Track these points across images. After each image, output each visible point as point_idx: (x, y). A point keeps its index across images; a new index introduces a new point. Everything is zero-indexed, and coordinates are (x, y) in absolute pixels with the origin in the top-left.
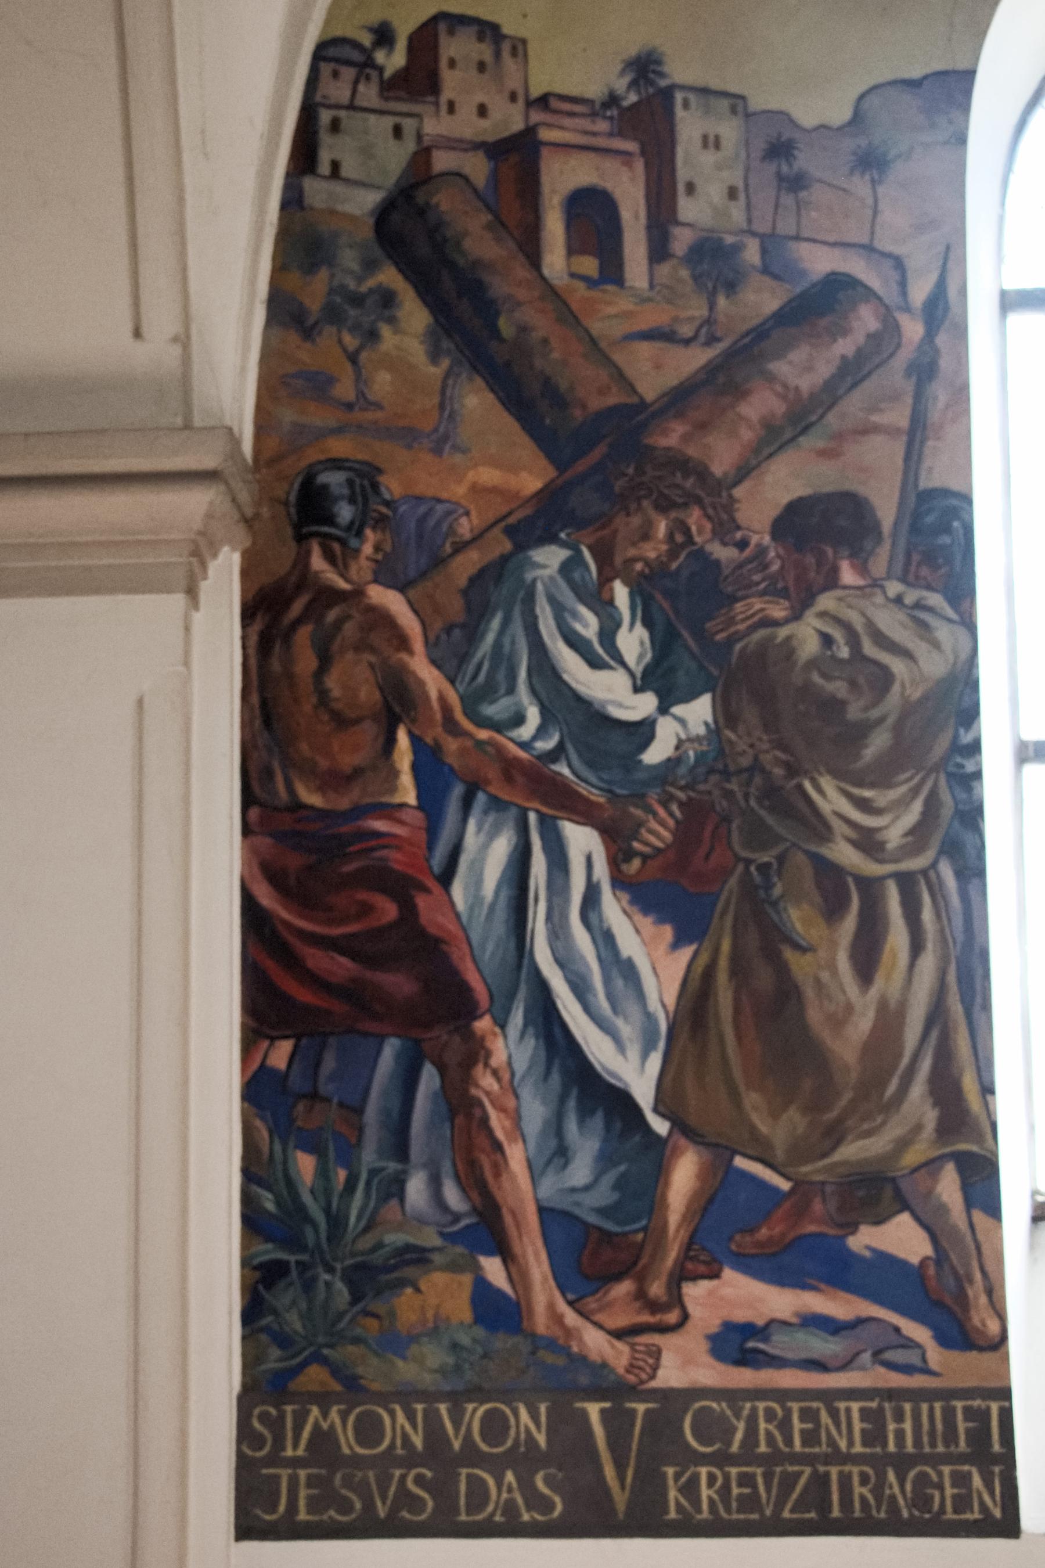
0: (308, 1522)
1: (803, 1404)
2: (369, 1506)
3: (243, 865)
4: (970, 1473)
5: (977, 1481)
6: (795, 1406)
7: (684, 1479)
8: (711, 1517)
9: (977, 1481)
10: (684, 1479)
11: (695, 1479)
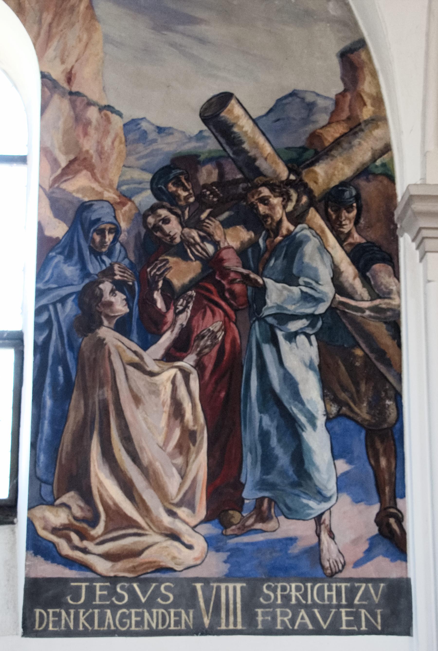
0: (53, 631)
1: (282, 609)
2: (198, 617)
3: (159, 498)
4: (181, 612)
5: (184, 615)
6: (98, 585)
7: (87, 614)
8: (148, 629)
9: (146, 615)
10: (87, 614)
11: (92, 614)
